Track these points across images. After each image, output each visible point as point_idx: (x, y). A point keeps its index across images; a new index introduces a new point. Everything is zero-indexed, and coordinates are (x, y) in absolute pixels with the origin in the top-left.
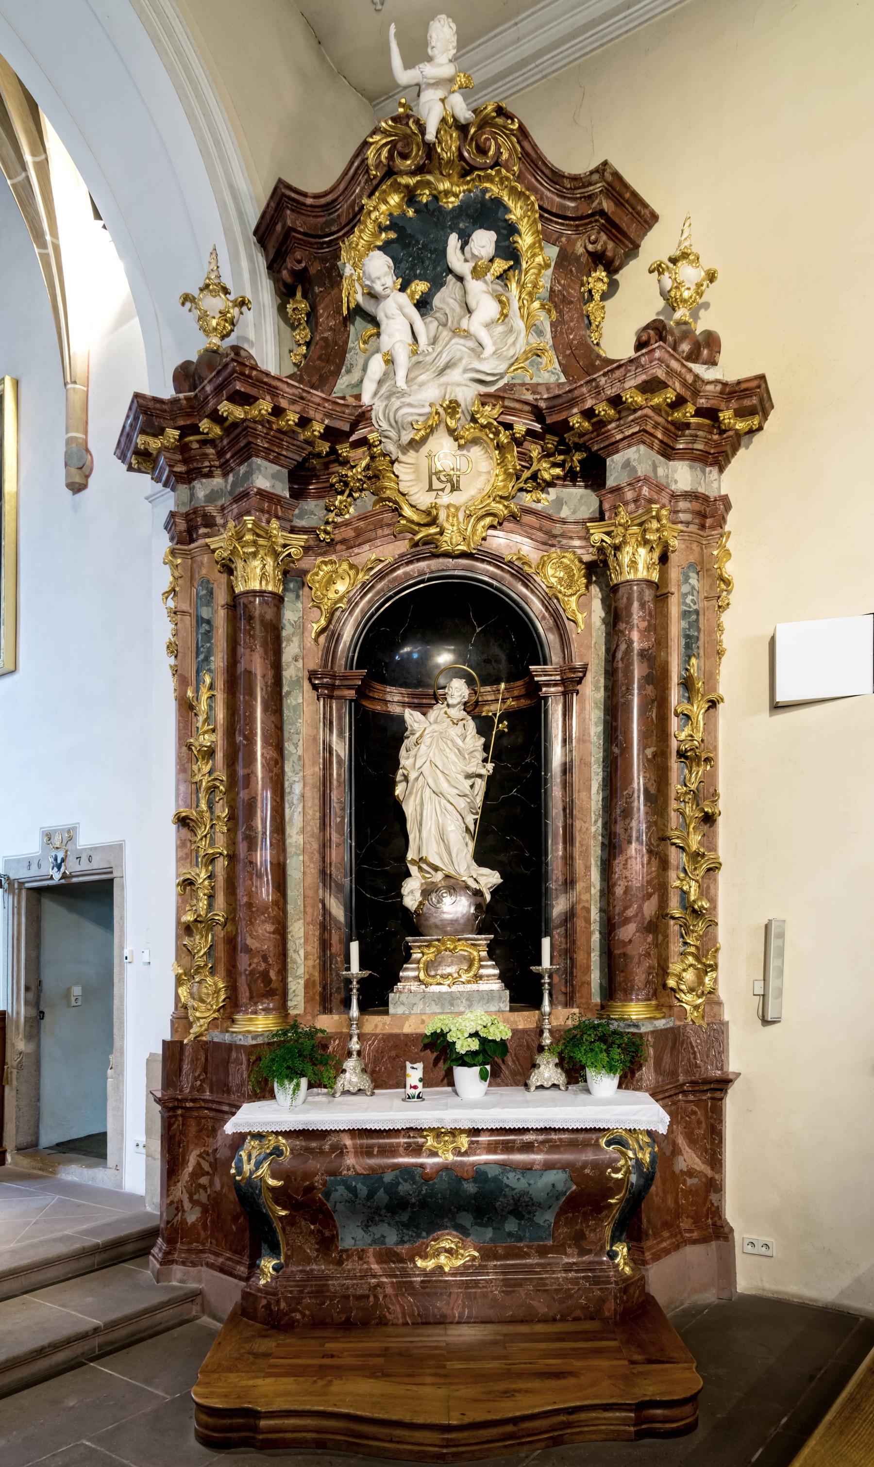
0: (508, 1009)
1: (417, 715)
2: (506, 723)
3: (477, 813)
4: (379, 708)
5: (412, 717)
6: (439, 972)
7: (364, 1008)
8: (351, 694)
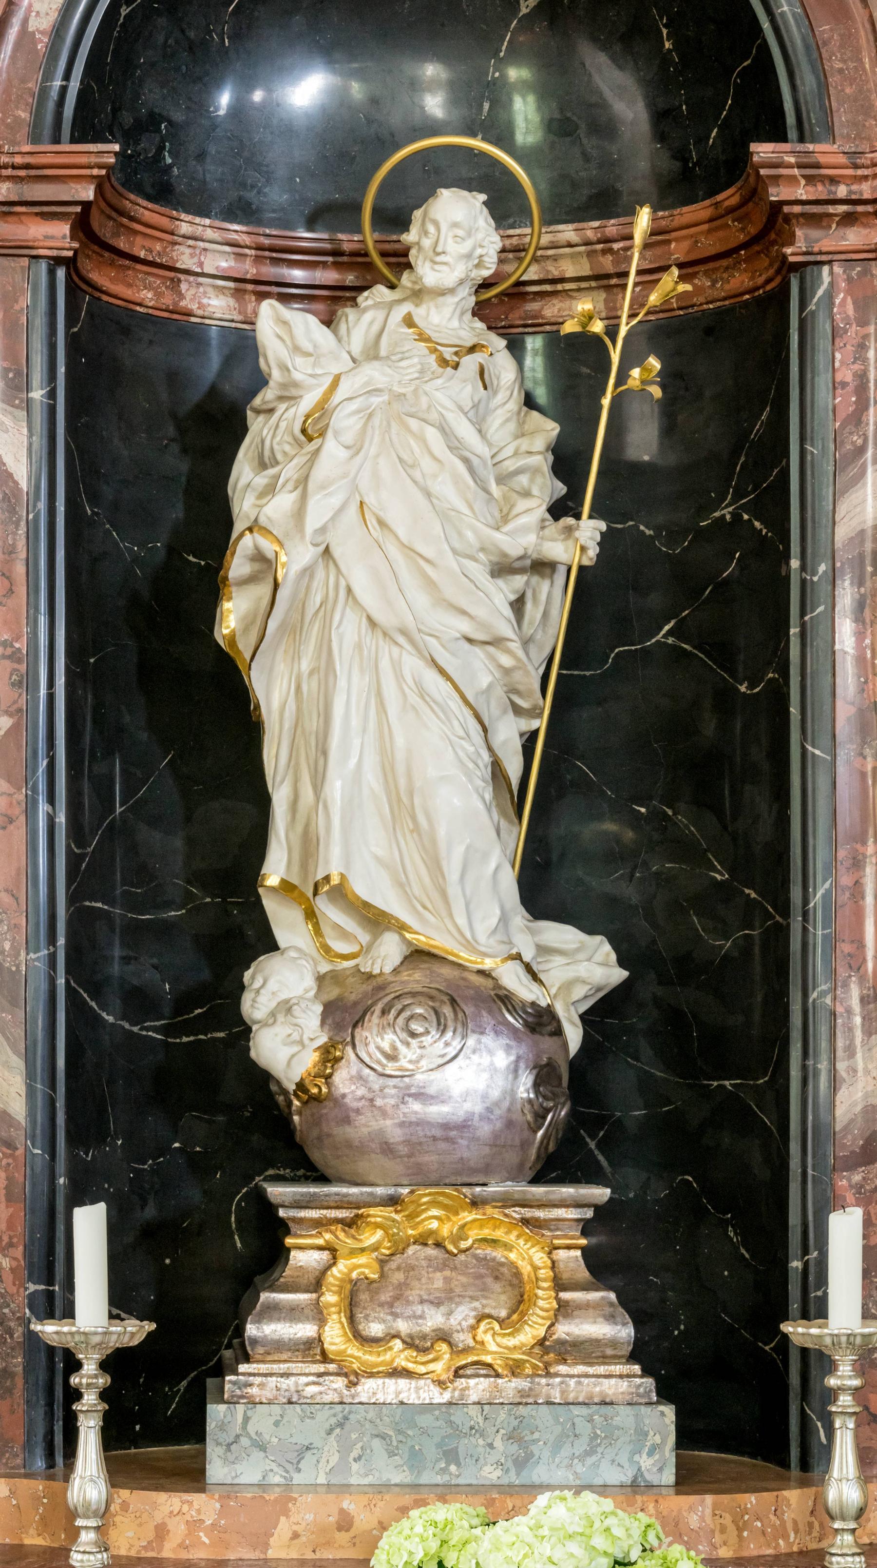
0: (669, 1477)
1: (305, 323)
2: (654, 363)
3: (19, 661)
4: (147, 296)
5: (284, 333)
6: (403, 1326)
7: (118, 1472)
8: (57, 235)
